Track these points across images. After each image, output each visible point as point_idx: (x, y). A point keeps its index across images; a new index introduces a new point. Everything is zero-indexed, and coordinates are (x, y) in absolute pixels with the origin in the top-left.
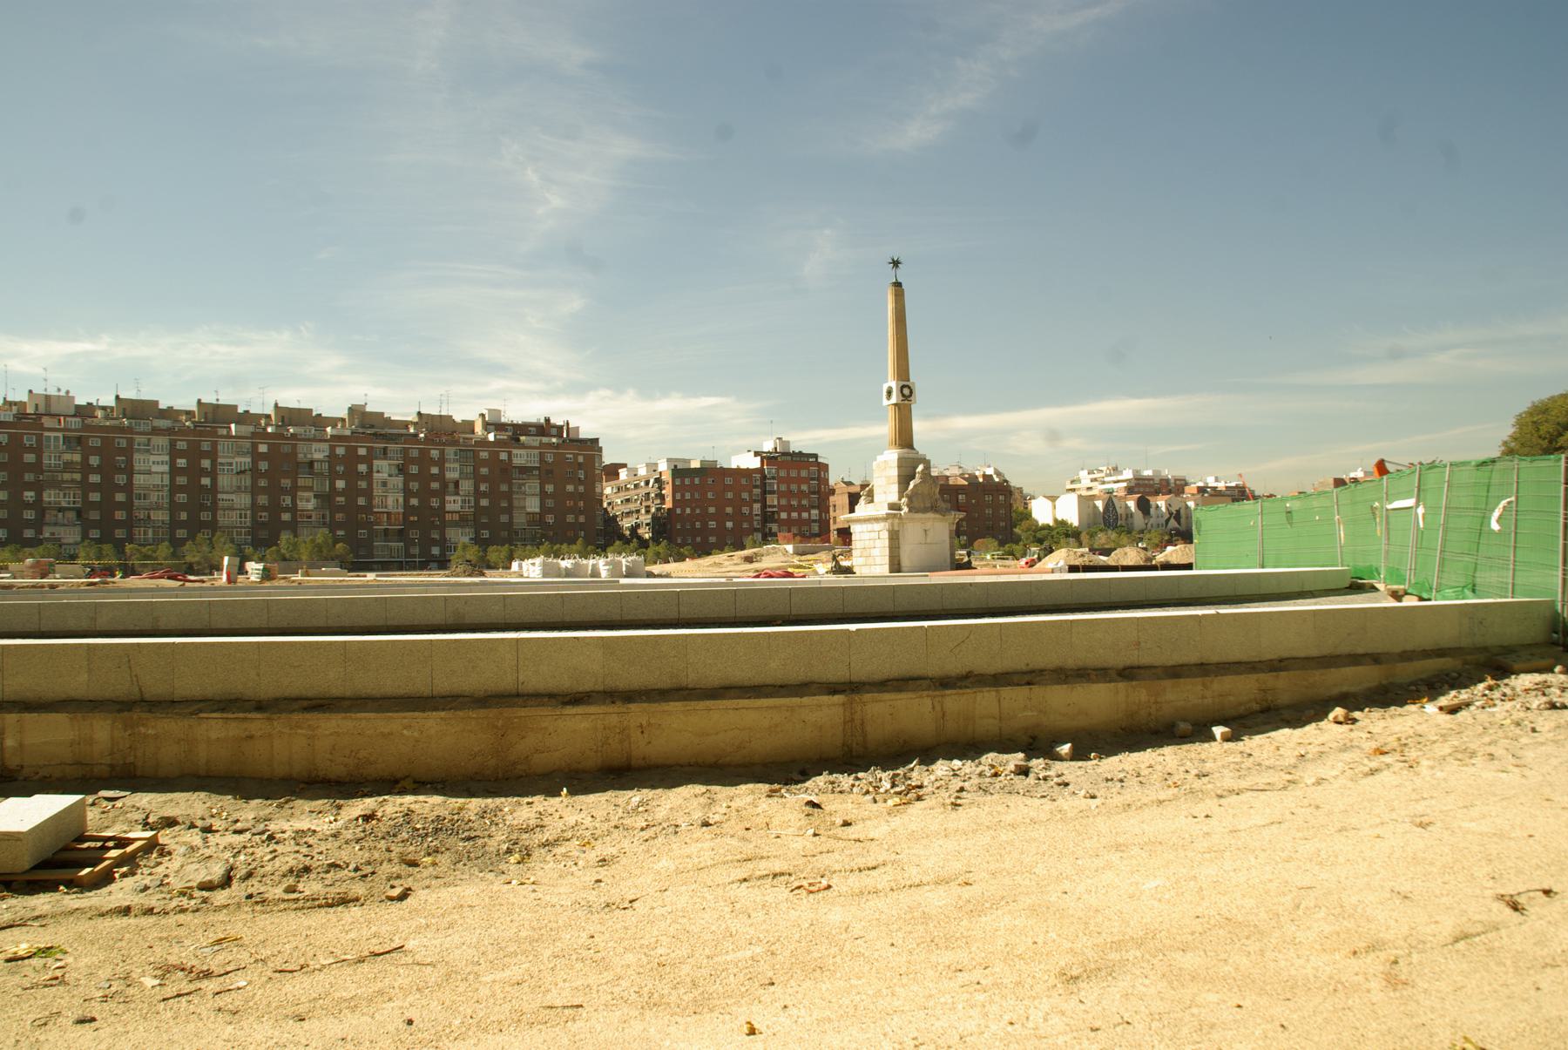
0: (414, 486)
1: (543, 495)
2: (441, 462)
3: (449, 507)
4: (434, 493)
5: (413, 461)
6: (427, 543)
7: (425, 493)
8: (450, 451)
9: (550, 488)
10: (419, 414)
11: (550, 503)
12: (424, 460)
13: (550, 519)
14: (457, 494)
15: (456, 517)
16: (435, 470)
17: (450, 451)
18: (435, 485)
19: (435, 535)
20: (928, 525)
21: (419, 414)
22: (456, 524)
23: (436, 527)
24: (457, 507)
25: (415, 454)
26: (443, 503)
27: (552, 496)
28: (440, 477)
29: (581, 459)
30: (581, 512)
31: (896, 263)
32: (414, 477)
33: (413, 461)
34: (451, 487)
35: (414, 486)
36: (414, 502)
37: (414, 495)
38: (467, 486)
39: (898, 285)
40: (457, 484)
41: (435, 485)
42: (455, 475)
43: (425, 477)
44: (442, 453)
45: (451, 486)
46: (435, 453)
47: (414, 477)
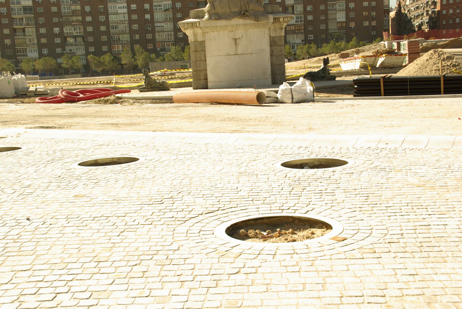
1: (348, 10)
9: (352, 5)
11: (352, 15)
13: (352, 25)
14: (293, 13)
20: (239, 33)
27: (353, 10)
34: (290, 9)
40: (293, 7)
45: (290, 9)
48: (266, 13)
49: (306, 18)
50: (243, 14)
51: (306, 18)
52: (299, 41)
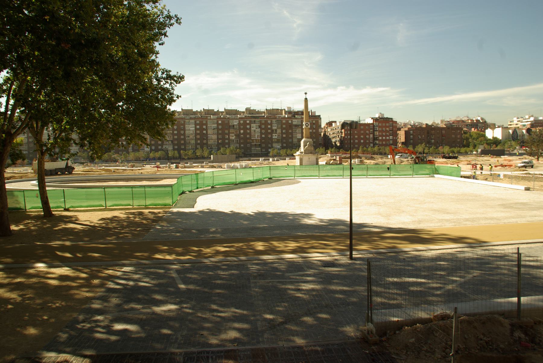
0: (263, 131)
2: (271, 124)
3: (274, 137)
4: (269, 133)
5: (263, 124)
6: (267, 148)
7: (266, 133)
8: (274, 121)
12: (266, 124)
15: (276, 140)
16: (269, 127)
17: (274, 121)
18: (269, 131)
22: (276, 142)
24: (276, 137)
25: (263, 122)
26: (272, 136)
28: (271, 129)
29: (314, 122)
31: (306, 93)
32: (263, 129)
33: (263, 124)
35: (263, 131)
36: (263, 136)
37: (263, 134)
38: (279, 131)
39: (306, 99)
40: (276, 130)
41: (269, 131)
42: (276, 128)
43: (266, 129)
44: (272, 121)
46: (269, 122)
47: (263, 129)
49: (282, 136)
50: (311, 153)
51: (282, 136)
52: (279, 147)
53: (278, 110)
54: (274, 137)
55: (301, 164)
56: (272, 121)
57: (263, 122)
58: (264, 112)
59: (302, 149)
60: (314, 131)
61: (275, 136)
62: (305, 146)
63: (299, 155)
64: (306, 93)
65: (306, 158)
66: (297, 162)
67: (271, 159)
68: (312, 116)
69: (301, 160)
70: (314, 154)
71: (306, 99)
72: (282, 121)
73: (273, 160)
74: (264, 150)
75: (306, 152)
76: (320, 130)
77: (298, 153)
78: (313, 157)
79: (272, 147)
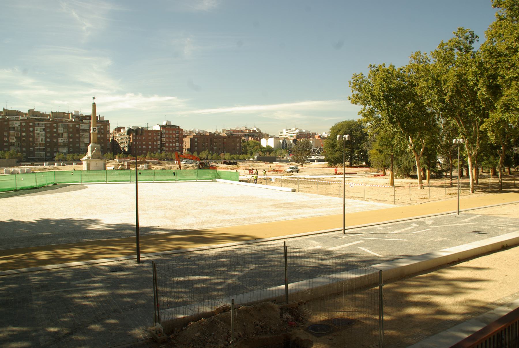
0: (48, 135)
2: (57, 128)
3: (59, 141)
4: (55, 137)
5: (48, 127)
7: (52, 137)
8: (60, 124)
10: (4, 109)
12: (51, 127)
16: (55, 130)
17: (60, 124)
18: (55, 135)
19: (55, 150)
20: (97, 162)
21: (4, 109)
22: (62, 147)
23: (55, 148)
24: (62, 141)
25: (49, 125)
26: (58, 140)
28: (57, 132)
29: (102, 127)
30: (102, 143)
31: (94, 98)
33: (48, 127)
36: (48, 140)
37: (48, 138)
38: (65, 135)
39: (94, 104)
40: (62, 134)
41: (55, 135)
42: (62, 132)
43: (52, 132)
44: (57, 125)
45: (61, 135)
46: (55, 125)
47: (48, 132)
48: (103, 158)
49: (69, 140)
50: (99, 158)
51: (69, 140)
52: (65, 151)
53: (65, 113)
54: (59, 141)
55: (88, 169)
56: (57, 125)
57: (49, 125)
58: (49, 115)
59: (89, 154)
60: (102, 136)
61: (61, 140)
62: (92, 151)
63: (86, 160)
64: (94, 98)
65: (93, 163)
66: (84, 167)
67: (56, 164)
68: (100, 121)
69: (88, 165)
70: (101, 159)
71: (94, 104)
72: (68, 125)
73: (59, 165)
74: (48, 155)
75: (94, 157)
76: (108, 135)
77: (85, 158)
78: (100, 163)
79: (58, 151)
